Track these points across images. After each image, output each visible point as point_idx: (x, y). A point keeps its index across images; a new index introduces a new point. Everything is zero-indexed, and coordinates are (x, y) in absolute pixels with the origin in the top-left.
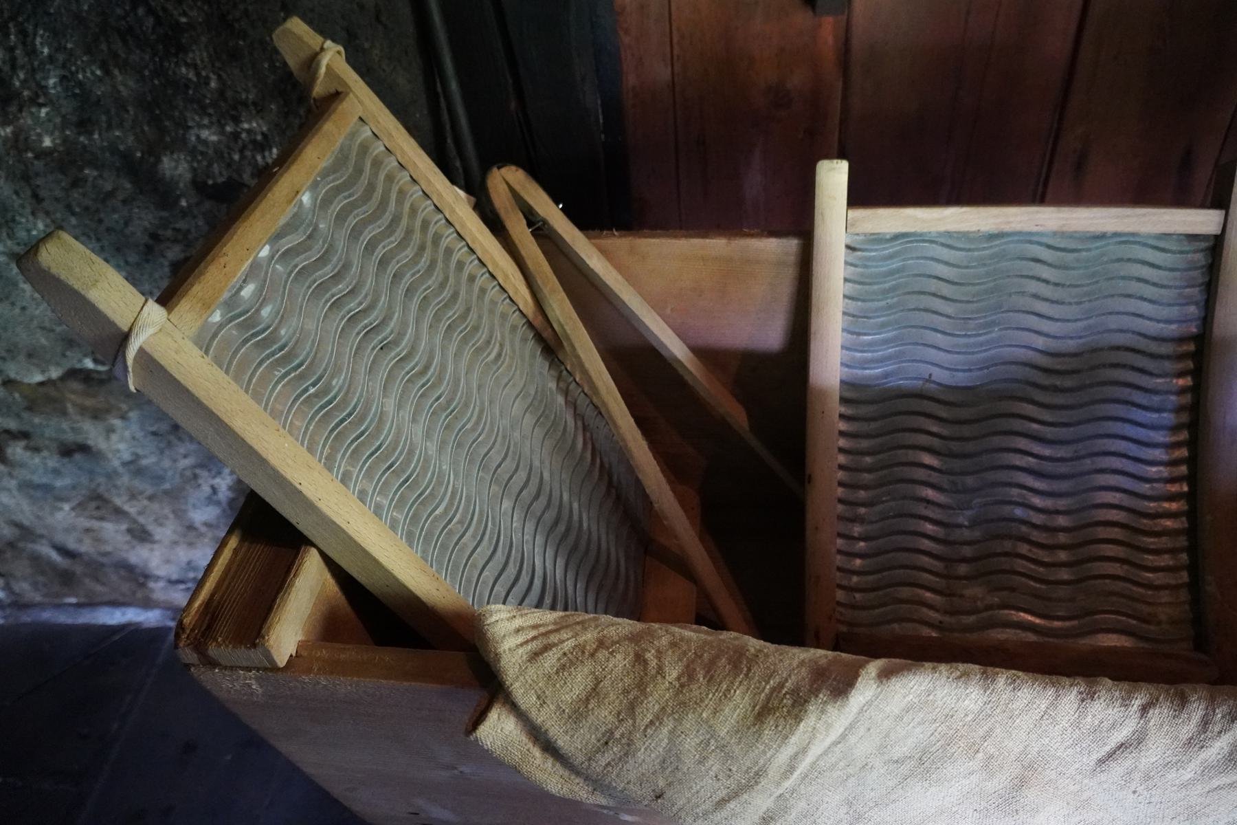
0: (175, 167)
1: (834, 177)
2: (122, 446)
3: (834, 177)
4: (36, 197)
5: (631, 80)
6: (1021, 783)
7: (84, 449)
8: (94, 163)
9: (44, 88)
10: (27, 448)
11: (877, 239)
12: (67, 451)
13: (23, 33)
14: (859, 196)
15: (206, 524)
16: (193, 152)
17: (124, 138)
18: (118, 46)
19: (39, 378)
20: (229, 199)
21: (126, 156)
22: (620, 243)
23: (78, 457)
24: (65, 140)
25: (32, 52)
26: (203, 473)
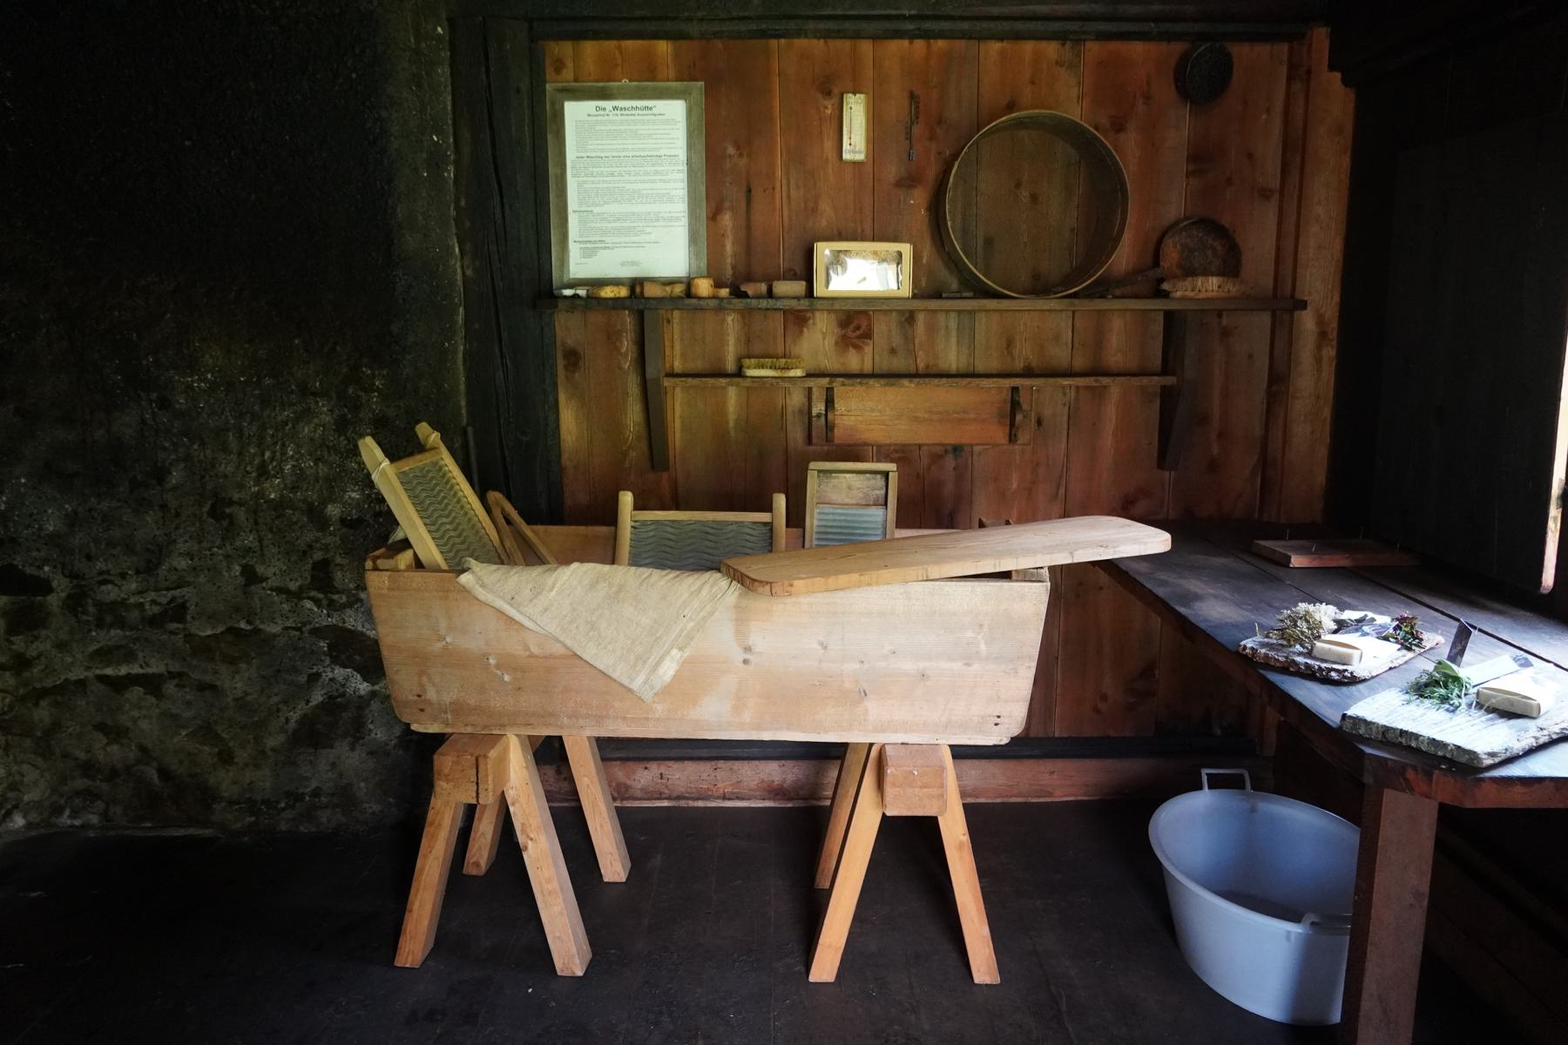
0: (333, 511)
1: (627, 499)
2: (239, 685)
3: (627, 499)
4: (256, 523)
5: (568, 502)
6: (617, 592)
7: (213, 687)
8: (294, 508)
9: (282, 470)
10: (177, 685)
11: (644, 523)
12: (202, 687)
13: (283, 445)
14: (637, 507)
15: (272, 750)
16: (344, 504)
17: (313, 496)
18: (325, 453)
19: (209, 632)
20: (399, 458)
21: (310, 505)
22: (541, 528)
23: (207, 693)
24: (282, 496)
25: (284, 454)
26: (283, 708)
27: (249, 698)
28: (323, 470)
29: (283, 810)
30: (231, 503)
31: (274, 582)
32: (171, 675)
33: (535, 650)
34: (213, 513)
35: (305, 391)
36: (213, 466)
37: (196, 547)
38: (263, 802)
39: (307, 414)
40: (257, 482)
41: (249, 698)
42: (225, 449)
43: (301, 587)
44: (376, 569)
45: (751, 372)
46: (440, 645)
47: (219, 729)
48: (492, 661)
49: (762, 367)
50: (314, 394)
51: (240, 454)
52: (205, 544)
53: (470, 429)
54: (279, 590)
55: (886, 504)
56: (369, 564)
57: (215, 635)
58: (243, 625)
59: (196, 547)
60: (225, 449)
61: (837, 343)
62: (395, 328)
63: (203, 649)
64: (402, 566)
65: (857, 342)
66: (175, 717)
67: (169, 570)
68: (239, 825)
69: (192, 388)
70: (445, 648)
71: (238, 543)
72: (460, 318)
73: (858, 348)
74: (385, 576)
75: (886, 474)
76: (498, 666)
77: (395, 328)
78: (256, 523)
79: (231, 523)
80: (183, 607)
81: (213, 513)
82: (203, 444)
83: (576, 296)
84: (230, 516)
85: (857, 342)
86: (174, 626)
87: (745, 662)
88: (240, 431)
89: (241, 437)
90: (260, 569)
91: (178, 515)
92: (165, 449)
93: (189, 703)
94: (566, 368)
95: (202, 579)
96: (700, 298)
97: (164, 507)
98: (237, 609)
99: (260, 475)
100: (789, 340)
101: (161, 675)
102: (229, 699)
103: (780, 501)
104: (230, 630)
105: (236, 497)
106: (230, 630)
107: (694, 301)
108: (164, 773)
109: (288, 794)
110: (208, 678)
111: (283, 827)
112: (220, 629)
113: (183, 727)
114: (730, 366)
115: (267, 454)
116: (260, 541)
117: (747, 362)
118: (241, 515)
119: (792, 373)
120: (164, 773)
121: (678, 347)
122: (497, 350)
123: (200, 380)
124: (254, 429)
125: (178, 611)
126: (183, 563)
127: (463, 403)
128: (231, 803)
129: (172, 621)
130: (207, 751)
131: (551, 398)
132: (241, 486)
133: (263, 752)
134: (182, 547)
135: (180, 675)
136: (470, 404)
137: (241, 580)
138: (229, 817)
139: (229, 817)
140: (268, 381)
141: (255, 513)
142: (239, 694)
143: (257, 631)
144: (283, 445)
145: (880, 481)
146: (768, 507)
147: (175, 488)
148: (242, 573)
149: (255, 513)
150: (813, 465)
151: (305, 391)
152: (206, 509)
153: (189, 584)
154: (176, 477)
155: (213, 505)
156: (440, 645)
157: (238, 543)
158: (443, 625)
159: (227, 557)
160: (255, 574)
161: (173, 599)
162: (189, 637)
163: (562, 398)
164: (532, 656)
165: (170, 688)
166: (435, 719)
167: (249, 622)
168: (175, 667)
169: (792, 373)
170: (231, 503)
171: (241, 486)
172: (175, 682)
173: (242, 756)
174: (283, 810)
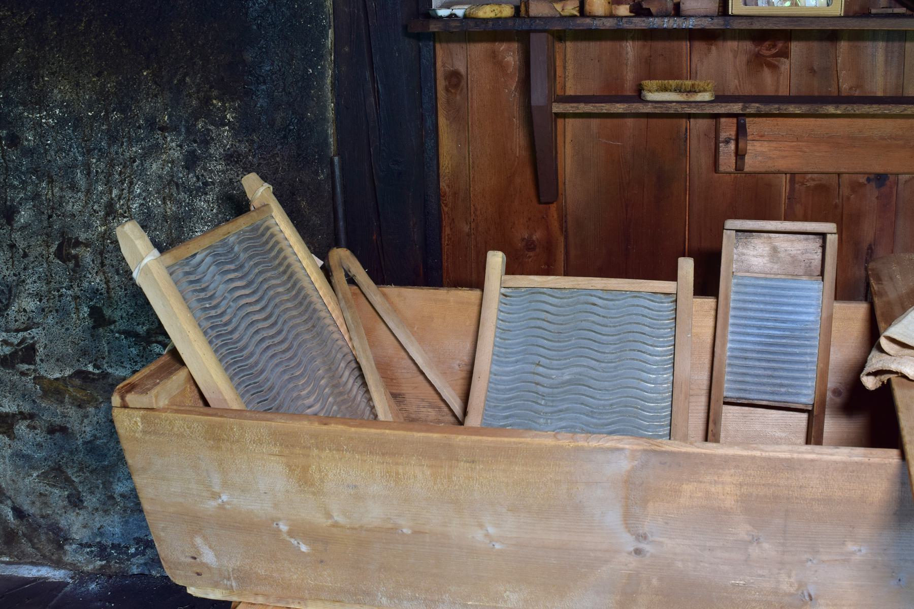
2: (88, 429)
3: (496, 260)
4: (102, 264)
7: (63, 430)
10: (28, 426)
13: (131, 183)
14: (510, 269)
15: (122, 496)
18: (174, 190)
25: (130, 192)
27: (98, 442)
28: (171, 208)
29: (134, 555)
30: (77, 243)
31: (121, 325)
32: (23, 416)
33: (339, 518)
34: (59, 254)
35: (152, 124)
36: (60, 205)
37: (45, 288)
38: (114, 546)
39: (154, 150)
40: (105, 222)
41: (98, 442)
42: (74, 187)
43: (148, 331)
44: (125, 406)
45: (651, 96)
46: (213, 504)
47: (69, 472)
48: (284, 528)
49: (665, 89)
50: (163, 129)
51: (88, 192)
52: (52, 285)
53: (336, 159)
54: (128, 334)
55: (822, 274)
56: (116, 400)
57: (63, 379)
58: (90, 368)
59: (45, 288)
60: (74, 187)
61: (749, 62)
62: (249, 56)
63: (54, 391)
64: (163, 402)
65: (773, 61)
66: (27, 458)
67: (19, 311)
68: (90, 567)
69: (41, 125)
70: (222, 507)
71: (85, 285)
72: (330, 42)
73: (774, 67)
74: (137, 417)
75: (823, 236)
76: (291, 533)
77: (249, 56)
78: (102, 264)
79: (77, 265)
80: (32, 349)
81: (59, 254)
82: (51, 181)
83: (452, 16)
84: (76, 257)
85: (773, 61)
86: (25, 367)
87: (638, 552)
88: (87, 166)
89: (89, 174)
90: (107, 312)
91: (25, 255)
92: (15, 187)
93: (40, 445)
94: (447, 90)
95: (50, 320)
96: (594, 17)
97: (12, 246)
98: (84, 353)
99: (107, 214)
100: (695, 59)
101: (14, 415)
102: (80, 442)
103: (686, 267)
104: (79, 374)
105: (83, 237)
106: (79, 374)
107: (588, 21)
108: (19, 513)
109: (138, 541)
110: (58, 421)
111: (135, 570)
112: (68, 373)
113: (34, 468)
114: (629, 89)
115: (115, 192)
116: (107, 282)
117: (647, 83)
118: (87, 256)
119: (700, 97)
120: (19, 513)
121: (570, 66)
122: (368, 74)
123: (49, 116)
124: (102, 166)
125: (28, 353)
126: (30, 305)
127: (331, 131)
128: (82, 545)
129: (22, 362)
130: (58, 496)
131: (429, 123)
132: (88, 226)
133: (111, 497)
134: (31, 286)
135: (31, 416)
136: (339, 129)
137: (89, 323)
138: (80, 558)
139: (80, 558)
140: (116, 116)
141: (101, 253)
142: (88, 437)
143: (105, 375)
144: (131, 183)
145: (814, 245)
146: (672, 276)
147: (23, 228)
148: (91, 315)
149: (101, 253)
150: (731, 224)
151: (152, 124)
152: (53, 249)
153: (38, 325)
154: (24, 216)
155: (60, 246)
156: (213, 504)
157: (85, 285)
158: (216, 480)
159: (76, 298)
160: (103, 316)
161: (23, 340)
162: (38, 379)
163: (442, 121)
164: (336, 525)
165: (21, 427)
166: (216, 585)
167: (95, 366)
168: (26, 408)
169: (700, 97)
170: (77, 243)
171: (88, 226)
172: (27, 422)
173: (91, 501)
174: (134, 555)
